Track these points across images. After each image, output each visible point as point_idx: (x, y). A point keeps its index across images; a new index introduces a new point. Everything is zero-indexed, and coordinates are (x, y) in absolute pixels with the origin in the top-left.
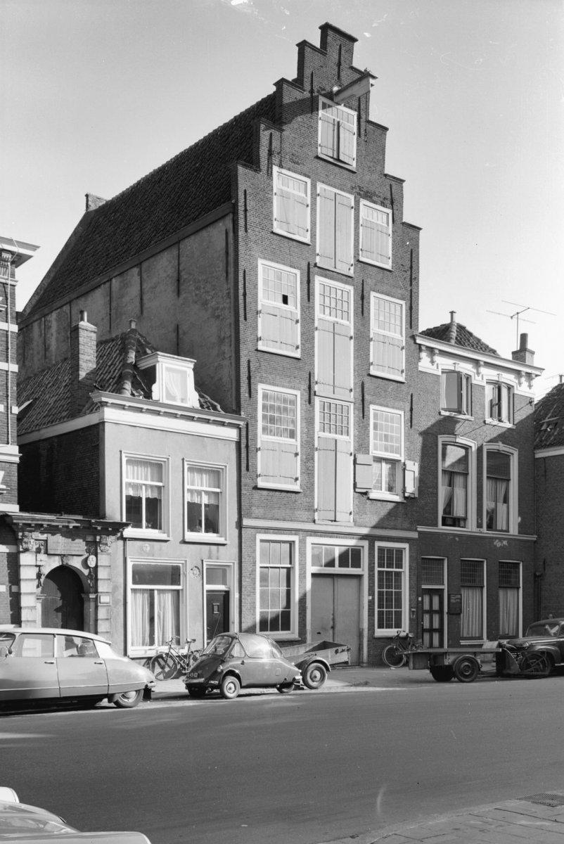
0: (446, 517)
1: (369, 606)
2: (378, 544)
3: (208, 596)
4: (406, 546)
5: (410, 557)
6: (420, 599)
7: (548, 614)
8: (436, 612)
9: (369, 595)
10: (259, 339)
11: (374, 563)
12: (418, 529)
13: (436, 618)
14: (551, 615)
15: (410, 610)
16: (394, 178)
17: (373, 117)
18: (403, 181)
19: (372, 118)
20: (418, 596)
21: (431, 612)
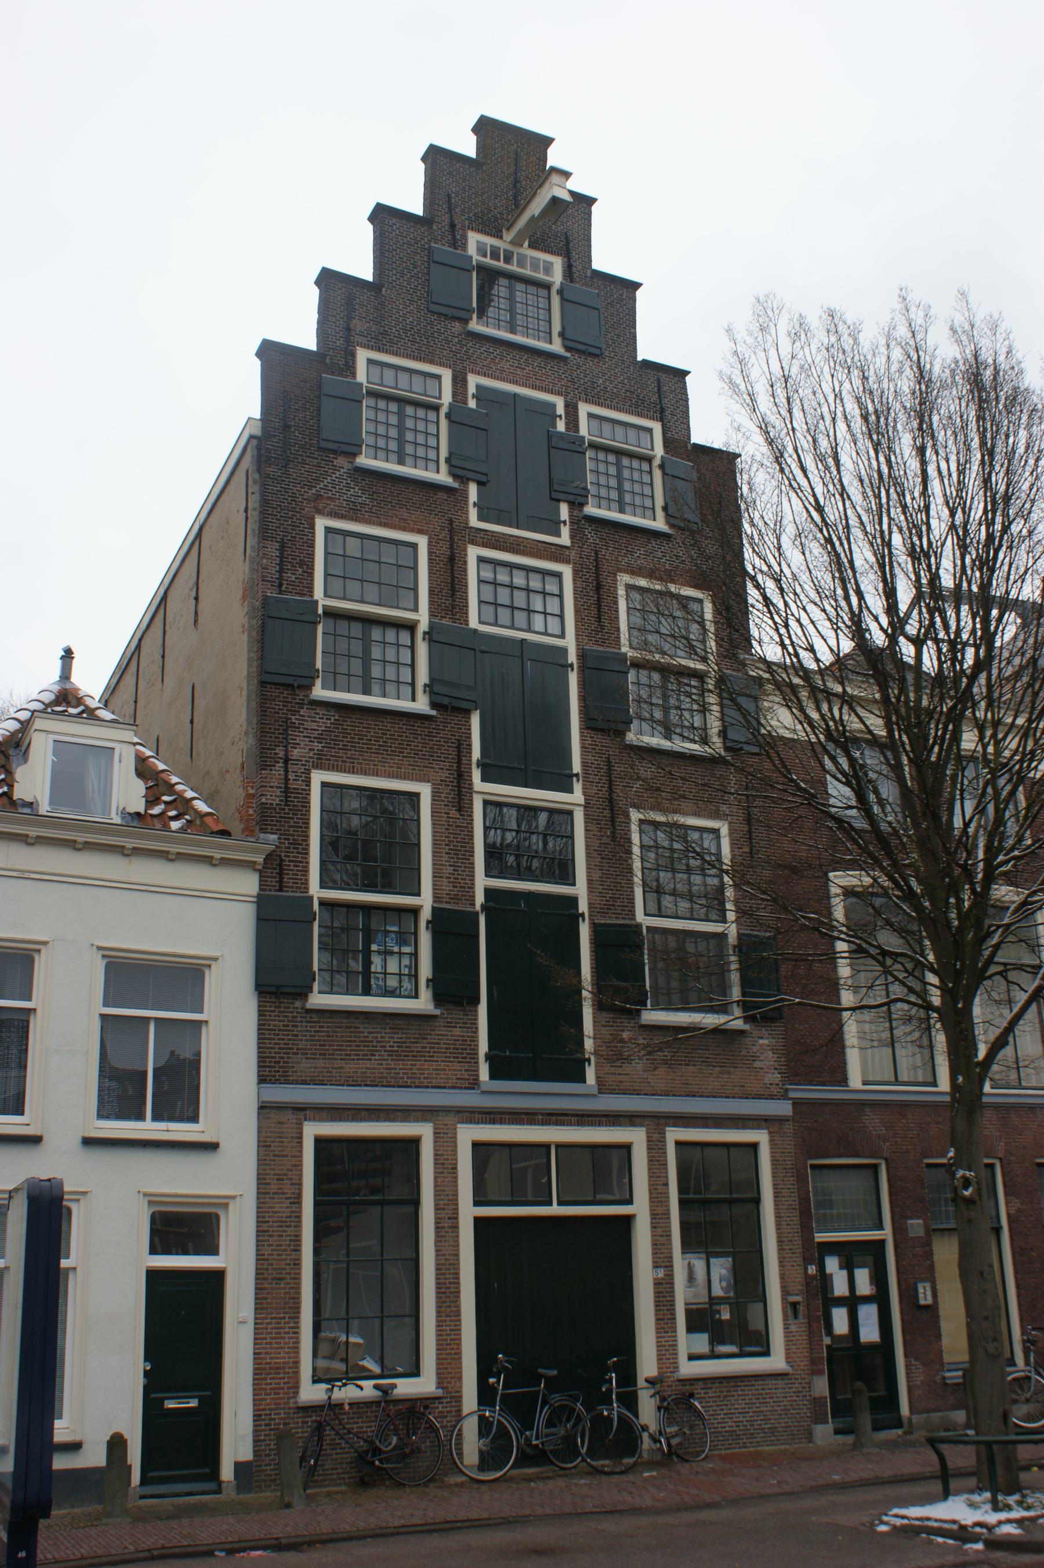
0: (1030, 1382)
1: (658, 1294)
2: (674, 1135)
3: (209, 1214)
4: (761, 1137)
5: (774, 1162)
6: (812, 1270)
7: (763, 735)
8: (866, 1300)
9: (656, 1266)
10: (65, 699)
11: (666, 1184)
12: (791, 1095)
13: (869, 1314)
14: (763, 731)
15: (784, 1299)
16: (713, 1097)
17: (600, 262)
18: (687, 373)
19: (598, 264)
20: (807, 1261)
21: (852, 1302)
